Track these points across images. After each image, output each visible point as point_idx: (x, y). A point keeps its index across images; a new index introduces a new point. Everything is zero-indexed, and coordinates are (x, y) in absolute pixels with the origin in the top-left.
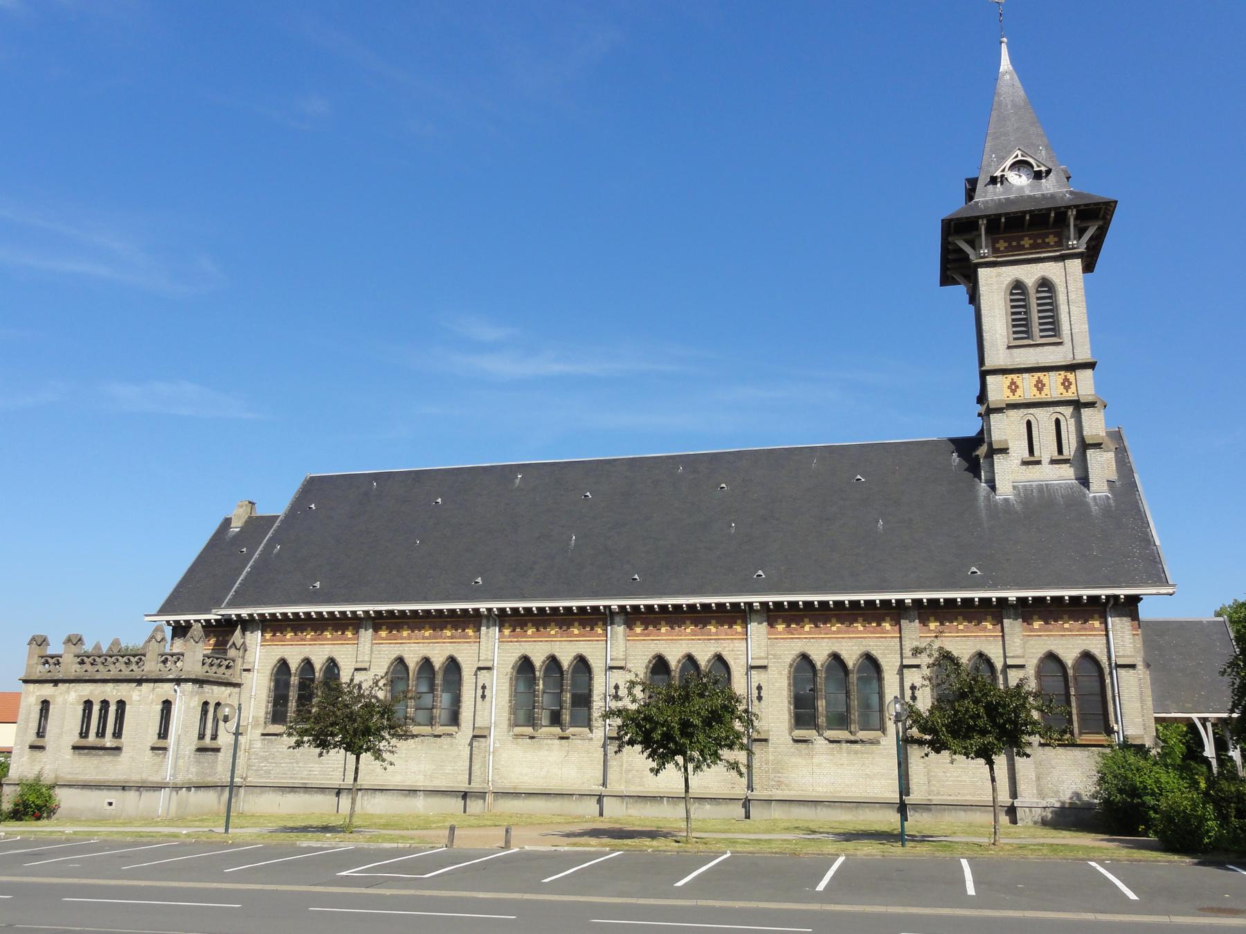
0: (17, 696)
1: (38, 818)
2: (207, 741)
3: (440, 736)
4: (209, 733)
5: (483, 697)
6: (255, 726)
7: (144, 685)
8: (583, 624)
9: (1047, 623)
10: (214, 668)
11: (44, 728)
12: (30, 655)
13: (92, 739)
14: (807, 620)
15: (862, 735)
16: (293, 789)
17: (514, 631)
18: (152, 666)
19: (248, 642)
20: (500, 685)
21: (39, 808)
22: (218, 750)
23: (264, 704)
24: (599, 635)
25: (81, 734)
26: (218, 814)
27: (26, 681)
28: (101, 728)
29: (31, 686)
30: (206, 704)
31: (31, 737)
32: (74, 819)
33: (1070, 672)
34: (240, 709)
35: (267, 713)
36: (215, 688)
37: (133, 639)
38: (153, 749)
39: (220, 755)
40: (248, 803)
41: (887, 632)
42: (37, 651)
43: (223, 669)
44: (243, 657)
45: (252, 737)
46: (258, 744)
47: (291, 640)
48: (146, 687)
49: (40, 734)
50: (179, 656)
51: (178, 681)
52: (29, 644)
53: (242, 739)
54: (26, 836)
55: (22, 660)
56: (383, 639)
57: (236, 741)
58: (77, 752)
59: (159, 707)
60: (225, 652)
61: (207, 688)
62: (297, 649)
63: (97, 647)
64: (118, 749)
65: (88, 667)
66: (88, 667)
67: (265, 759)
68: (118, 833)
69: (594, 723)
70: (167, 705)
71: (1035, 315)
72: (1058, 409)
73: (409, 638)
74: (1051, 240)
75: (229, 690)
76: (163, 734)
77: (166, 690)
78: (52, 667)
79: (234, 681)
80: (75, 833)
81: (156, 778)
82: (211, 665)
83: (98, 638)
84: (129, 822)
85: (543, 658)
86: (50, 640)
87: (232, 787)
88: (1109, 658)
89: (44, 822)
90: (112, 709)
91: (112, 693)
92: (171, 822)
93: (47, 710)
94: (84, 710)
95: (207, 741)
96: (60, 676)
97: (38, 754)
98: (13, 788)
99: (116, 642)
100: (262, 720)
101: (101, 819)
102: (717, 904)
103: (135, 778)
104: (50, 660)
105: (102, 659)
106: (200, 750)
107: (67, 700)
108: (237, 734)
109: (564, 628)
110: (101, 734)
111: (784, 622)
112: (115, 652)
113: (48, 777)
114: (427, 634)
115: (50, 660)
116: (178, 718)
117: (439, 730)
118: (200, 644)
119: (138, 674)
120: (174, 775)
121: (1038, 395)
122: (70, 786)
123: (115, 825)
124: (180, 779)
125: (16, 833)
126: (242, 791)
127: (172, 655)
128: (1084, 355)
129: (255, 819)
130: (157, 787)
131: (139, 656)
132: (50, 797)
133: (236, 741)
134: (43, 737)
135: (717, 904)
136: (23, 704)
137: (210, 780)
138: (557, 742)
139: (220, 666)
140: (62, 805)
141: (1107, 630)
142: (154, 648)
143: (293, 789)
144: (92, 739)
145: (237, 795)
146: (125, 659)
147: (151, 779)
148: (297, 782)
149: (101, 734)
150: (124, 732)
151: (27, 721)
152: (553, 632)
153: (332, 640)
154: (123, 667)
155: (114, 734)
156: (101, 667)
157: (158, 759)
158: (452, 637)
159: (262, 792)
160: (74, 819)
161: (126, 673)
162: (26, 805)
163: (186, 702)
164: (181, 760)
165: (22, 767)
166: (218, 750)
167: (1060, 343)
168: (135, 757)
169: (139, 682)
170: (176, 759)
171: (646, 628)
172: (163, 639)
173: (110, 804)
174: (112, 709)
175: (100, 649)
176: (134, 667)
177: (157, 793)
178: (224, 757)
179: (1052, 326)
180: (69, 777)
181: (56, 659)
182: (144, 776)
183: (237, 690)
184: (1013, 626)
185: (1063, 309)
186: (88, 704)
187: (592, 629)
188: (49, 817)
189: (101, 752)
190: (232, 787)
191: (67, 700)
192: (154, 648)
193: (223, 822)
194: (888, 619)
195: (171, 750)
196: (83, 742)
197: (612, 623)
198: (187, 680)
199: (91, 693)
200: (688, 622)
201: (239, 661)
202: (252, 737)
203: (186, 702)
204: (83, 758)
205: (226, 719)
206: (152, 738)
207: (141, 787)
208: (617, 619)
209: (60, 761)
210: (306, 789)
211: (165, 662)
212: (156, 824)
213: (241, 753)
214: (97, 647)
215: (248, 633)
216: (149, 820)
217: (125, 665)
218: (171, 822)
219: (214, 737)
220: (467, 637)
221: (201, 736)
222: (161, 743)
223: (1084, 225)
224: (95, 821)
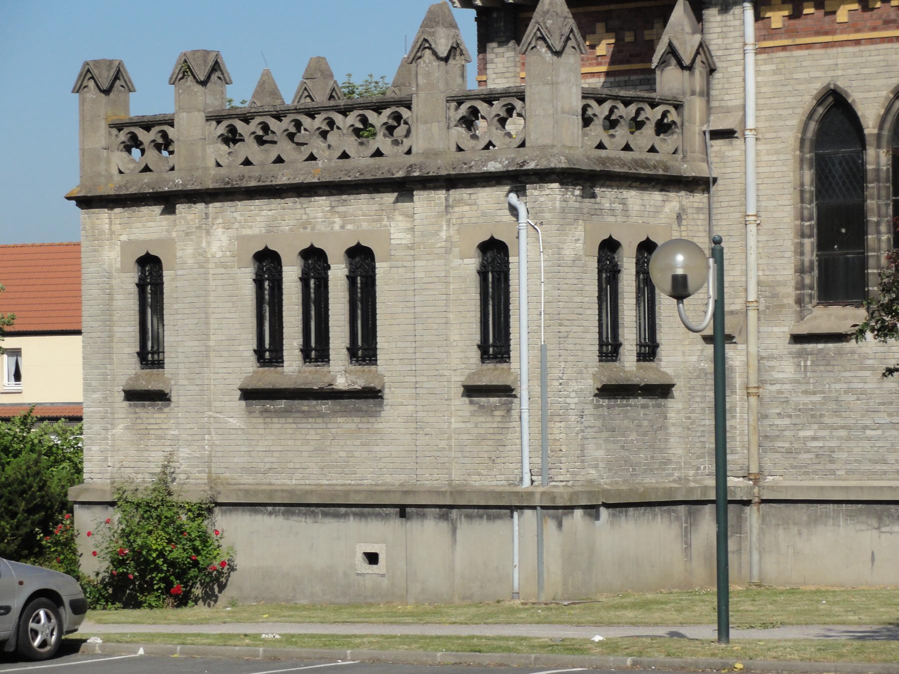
0: (71, 253)
1: (182, 601)
2: (629, 363)
4: (629, 336)
6: (771, 310)
7: (420, 197)
10: (622, 133)
11: (158, 340)
12: (86, 124)
13: (293, 368)
17: (796, 14)
18: (433, 138)
19: (715, 42)
21: (180, 570)
22: (663, 391)
23: (788, 241)
25: (259, 352)
26: (687, 588)
27: (86, 202)
28: (316, 328)
29: (103, 217)
30: (609, 247)
31: (126, 368)
32: (279, 603)
34: (718, 254)
35: (801, 270)
36: (633, 197)
37: (369, 62)
39: (675, 406)
40: (771, 552)
42: (104, 109)
43: (648, 133)
44: (706, 94)
45: (764, 344)
46: (785, 369)
48: (426, 202)
49: (150, 355)
50: (511, 102)
51: (518, 179)
52: (79, 88)
53: (735, 355)
54: (159, 646)
55: (64, 145)
57: (720, 361)
58: (257, 406)
59: (472, 263)
60: (648, 79)
61: (607, 196)
63: (266, 86)
65: (249, 148)
66: (249, 148)
67: (813, 415)
68: (406, 639)
70: (494, 256)
75: (675, 200)
76: (495, 343)
77: (486, 207)
78: (152, 155)
79: (688, 170)
80: (289, 639)
81: (490, 481)
82: (611, 123)
83: (266, 63)
84: (433, 608)
86: (133, 72)
87: (724, 504)
89: (201, 610)
90: (338, 273)
91: (332, 224)
92: (552, 609)
93: (158, 286)
94: (259, 282)
95: (629, 363)
96: (177, 182)
97: (149, 413)
98: (100, 514)
99: (318, 70)
100: (789, 293)
101: (355, 603)
103: (431, 479)
104: (145, 137)
105: (287, 123)
106: (611, 391)
107: (211, 250)
108: (719, 338)
110: (316, 350)
112: (321, 98)
113: (191, 486)
115: (145, 137)
116: (533, 296)
118: (570, 58)
119: (395, 163)
120: (543, 471)
122: (114, 623)
123: (394, 618)
124: (564, 480)
125: (135, 640)
126: (752, 514)
127: (489, 99)
129: (804, 601)
130: (501, 508)
131: (394, 108)
132: (204, 538)
133: (720, 361)
134: (160, 364)
136: (90, 273)
137: (653, 483)
139: (637, 124)
140: (240, 562)
142: (432, 86)
144: (293, 368)
145: (739, 530)
146: (353, 119)
147: (476, 482)
149: (316, 350)
150: (382, 342)
151: (108, 320)
154: (350, 144)
155: (352, 352)
156: (285, 148)
157: (488, 424)
159: (815, 521)
160: (279, 603)
161: (361, 163)
162: (144, 563)
163: (550, 245)
164: (552, 423)
165: (114, 456)
166: (663, 391)
168: (422, 423)
169: (404, 187)
170: (545, 419)
171: (796, 14)
172: (455, 50)
173: (372, 558)
174: (338, 273)
175: (275, 93)
176: (381, 142)
177: (499, 526)
178: (688, 409)
180: (248, 480)
181: (157, 133)
182: (457, 476)
183: (698, 199)
186: (267, 262)
188: (209, 597)
189: (324, 406)
190: (724, 504)
191: (211, 250)
192: (432, 86)
193: (708, 607)
195: (524, 393)
196: (270, 378)
198: (543, 176)
199: (271, 229)
201: (695, 106)
202: (764, 344)
203: (550, 245)
204: (277, 424)
205: (680, 289)
206: (462, 358)
207: (452, 508)
209: (207, 438)
211: (469, 121)
212: (511, 616)
213: (735, 399)
214: (266, 86)
215: (712, 15)
216: (492, 607)
217: (343, 141)
218: (552, 609)
219: (649, 351)
221: (609, 350)
222: (492, 375)
224: (339, 608)
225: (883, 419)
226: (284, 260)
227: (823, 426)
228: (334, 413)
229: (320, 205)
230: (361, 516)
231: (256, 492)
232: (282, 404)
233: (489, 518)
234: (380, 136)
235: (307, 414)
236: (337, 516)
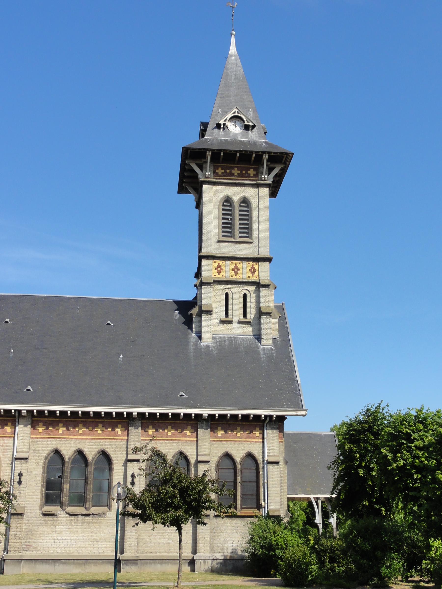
15: (94, 510)
33: (238, 466)
41: (119, 435)
71: (237, 222)
74: (252, 172)
111: (44, 425)
121: (234, 276)
128: (265, 252)
167: (251, 243)
179: (247, 230)
184: (204, 433)
187: (113, 430)
194: (120, 426)
220: (186, 435)
230: (65, 563)
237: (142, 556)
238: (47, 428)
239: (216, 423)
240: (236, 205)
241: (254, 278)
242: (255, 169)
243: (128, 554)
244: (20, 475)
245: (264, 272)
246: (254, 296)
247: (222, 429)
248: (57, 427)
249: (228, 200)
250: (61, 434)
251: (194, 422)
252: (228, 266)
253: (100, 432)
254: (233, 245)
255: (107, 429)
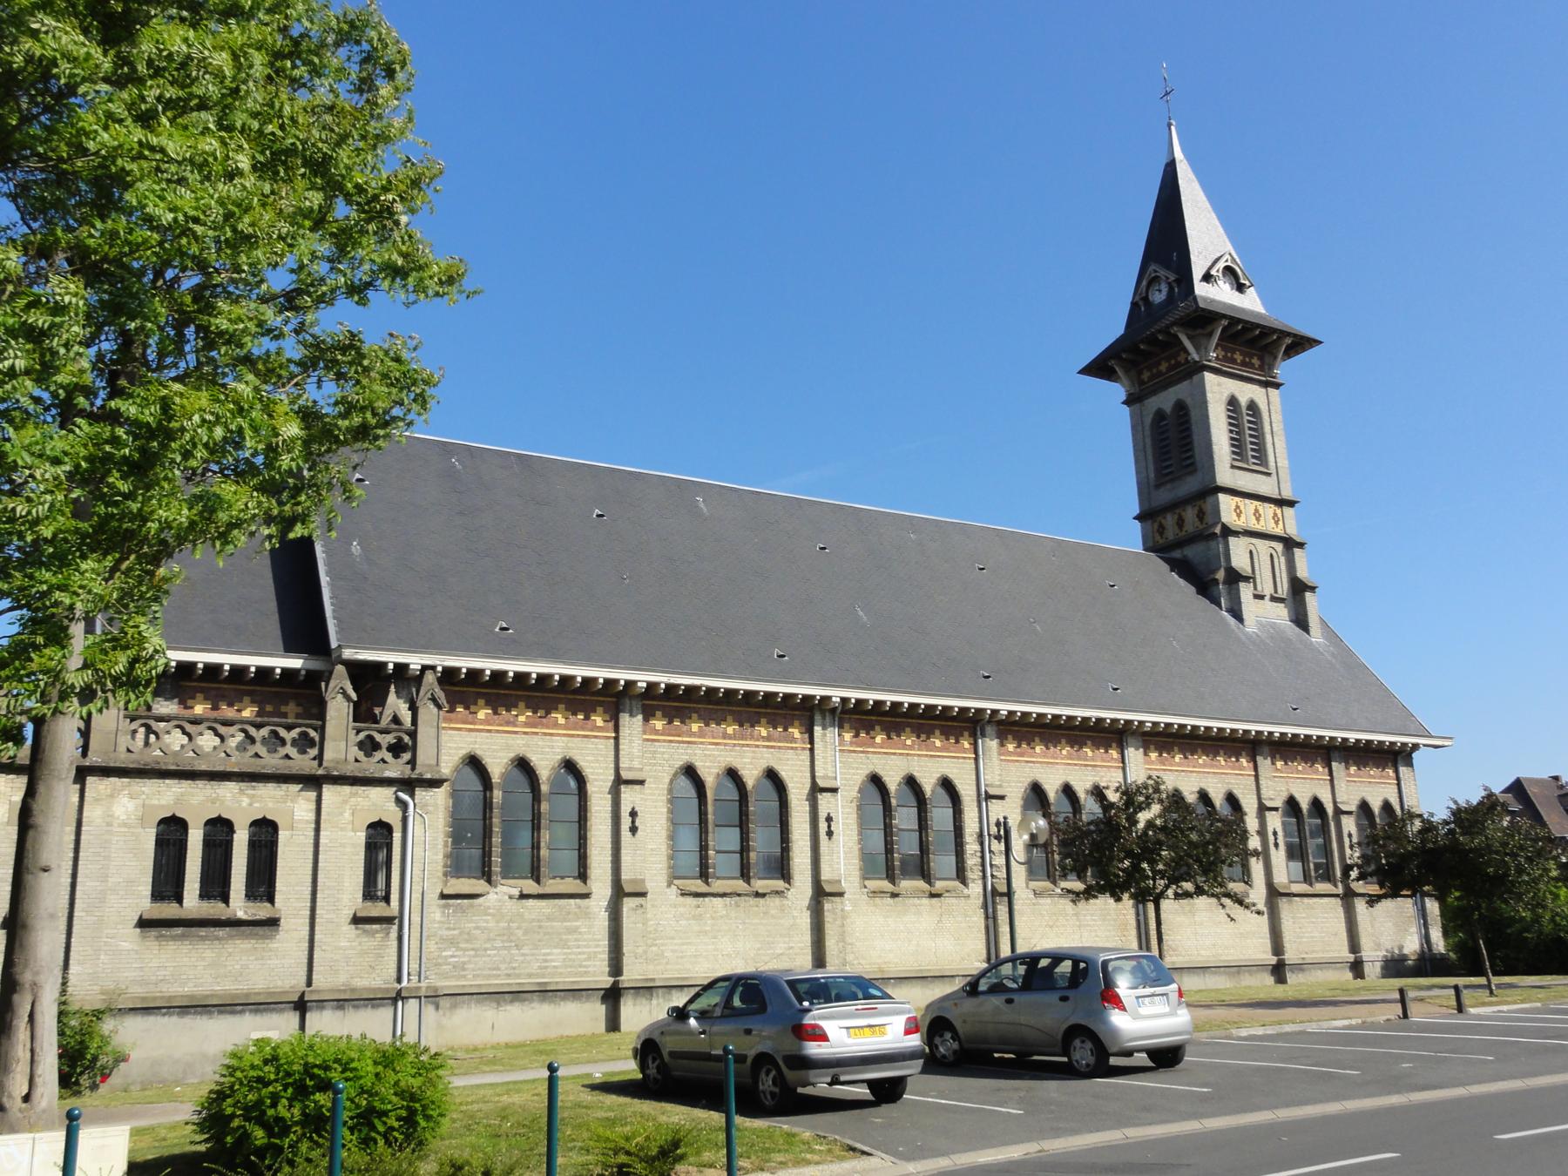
3: (763, 895)
5: (634, 830)
8: (946, 734)
9: (707, 725)
14: (481, 702)
16: (517, 995)
17: (857, 735)
20: (651, 806)
24: (965, 751)
33: (544, 788)
38: (357, 920)
41: (793, 740)
47: (486, 722)
56: (657, 732)
58: (154, 932)
62: (500, 740)
64: (273, 923)
67: (452, 942)
69: (970, 875)
72: (1274, 544)
73: (701, 734)
74: (1255, 361)
85: (933, 781)
88: (1335, 803)
102: (1477, 1089)
109: (923, 737)
114: (730, 730)
117: (760, 885)
122: (147, 1010)
135: (1477, 1089)
138: (926, 901)
141: (812, 742)
143: (517, 995)
144: (239, 905)
148: (528, 982)
152: (909, 742)
153: (565, 727)
158: (768, 738)
171: (1019, 746)
184: (826, 736)
185: (1268, 438)
186: (171, 831)
187: (587, 718)
194: (600, 710)
196: (169, 910)
197: (983, 735)
199: (178, 801)
200: (522, 705)
204: (172, 946)
208: (989, 730)
210: (545, 993)
223: (1209, 329)
225: (498, 944)
226: (190, 825)
227: (458, 949)
228: (231, 937)
229: (232, 787)
230: (256, 1011)
231: (155, 999)
232: (179, 931)
233: (373, 1007)
234: (258, 744)
235: (203, 938)
236: (233, 1013)
237: (1310, 957)
238: (670, 722)
239: (863, 719)
240: (1244, 411)
241: (1279, 531)
242: (1261, 359)
243: (630, 975)
244: (633, 814)
245: (1290, 523)
246: (1283, 559)
247: (488, 704)
248: (473, 708)
249: (1233, 402)
250: (482, 722)
251: (966, 726)
252: (1250, 506)
253: (561, 721)
254: (1248, 474)
255: (575, 714)
